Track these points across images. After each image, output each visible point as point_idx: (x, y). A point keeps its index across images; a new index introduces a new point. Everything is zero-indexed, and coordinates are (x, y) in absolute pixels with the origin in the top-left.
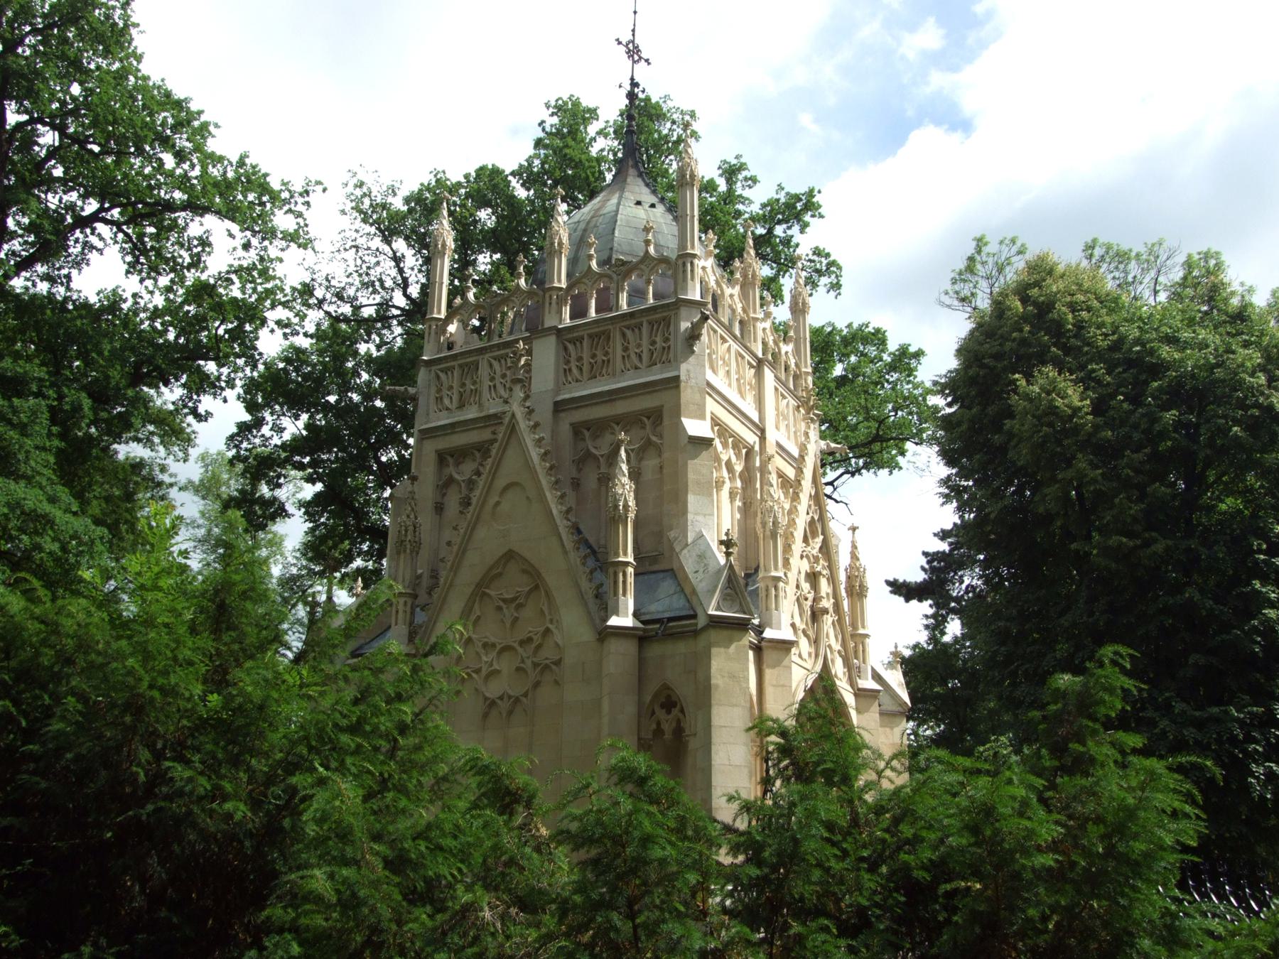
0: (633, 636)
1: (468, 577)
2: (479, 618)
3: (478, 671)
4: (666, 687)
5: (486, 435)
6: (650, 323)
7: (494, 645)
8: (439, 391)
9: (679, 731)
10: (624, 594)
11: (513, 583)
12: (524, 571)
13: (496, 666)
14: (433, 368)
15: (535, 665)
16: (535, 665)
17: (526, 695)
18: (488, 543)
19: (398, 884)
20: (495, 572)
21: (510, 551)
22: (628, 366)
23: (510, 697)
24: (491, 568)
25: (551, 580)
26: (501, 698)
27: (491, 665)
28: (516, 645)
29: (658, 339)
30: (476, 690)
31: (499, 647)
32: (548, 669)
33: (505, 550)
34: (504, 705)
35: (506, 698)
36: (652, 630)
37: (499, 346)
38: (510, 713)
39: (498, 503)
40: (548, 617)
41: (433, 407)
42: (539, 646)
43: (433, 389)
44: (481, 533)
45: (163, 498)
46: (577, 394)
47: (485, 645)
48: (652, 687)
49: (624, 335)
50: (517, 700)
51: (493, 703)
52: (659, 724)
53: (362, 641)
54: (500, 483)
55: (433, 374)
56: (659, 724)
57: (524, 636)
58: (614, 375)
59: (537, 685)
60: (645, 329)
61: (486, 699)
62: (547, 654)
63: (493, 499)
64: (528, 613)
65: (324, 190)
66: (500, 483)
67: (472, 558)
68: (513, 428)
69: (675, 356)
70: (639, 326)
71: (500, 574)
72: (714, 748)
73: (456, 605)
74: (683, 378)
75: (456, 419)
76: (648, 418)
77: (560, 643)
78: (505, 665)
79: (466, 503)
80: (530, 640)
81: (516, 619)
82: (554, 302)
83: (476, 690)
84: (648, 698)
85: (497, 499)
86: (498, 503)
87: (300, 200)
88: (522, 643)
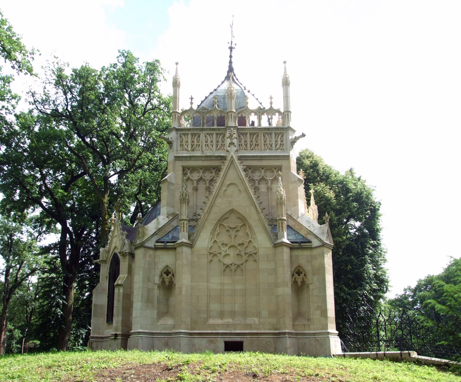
0: (289, 247)
1: (215, 216)
2: (219, 233)
3: (220, 253)
4: (299, 266)
5: (216, 163)
6: (216, 134)
7: (226, 245)
8: (181, 142)
9: (303, 282)
10: (283, 231)
11: (233, 222)
12: (238, 218)
13: (228, 252)
14: (179, 132)
15: (246, 254)
16: (246, 254)
17: (242, 264)
18: (221, 206)
19: (424, 372)
20: (225, 216)
21: (233, 209)
22: (266, 148)
23: (235, 265)
24: (225, 215)
25: (252, 222)
26: (231, 265)
27: (226, 252)
28: (237, 245)
29: (195, 141)
30: (219, 260)
31: (229, 245)
32: (253, 255)
33: (229, 209)
34: (233, 268)
35: (233, 265)
36: (294, 245)
37: (210, 129)
38: (235, 270)
39: (226, 190)
40: (250, 237)
41: (179, 148)
42: (247, 247)
43: (179, 141)
44: (219, 200)
45: (223, 163)
46: (247, 155)
47: (222, 244)
48: (295, 266)
49: (264, 136)
50: (238, 266)
51: (228, 266)
52: (295, 279)
53: (160, 237)
54: (227, 182)
55: (179, 135)
56: (295, 279)
57: (240, 242)
58: (261, 150)
59: (246, 261)
60: (273, 135)
61: (224, 264)
62: (249, 250)
63: (224, 189)
64: (240, 234)
65: (40, 54)
66: (227, 182)
67: (215, 209)
68: (232, 162)
69: (287, 149)
70: (271, 134)
71: (227, 218)
72: (327, 289)
73: (209, 227)
74: (291, 156)
75: (191, 155)
76: (275, 169)
77: (256, 246)
78: (232, 252)
79: (208, 189)
80: (243, 244)
81: (236, 236)
82: (233, 117)
83: (219, 260)
84: (293, 270)
85: (225, 188)
86: (226, 190)
87: (30, 56)
88: (239, 245)
